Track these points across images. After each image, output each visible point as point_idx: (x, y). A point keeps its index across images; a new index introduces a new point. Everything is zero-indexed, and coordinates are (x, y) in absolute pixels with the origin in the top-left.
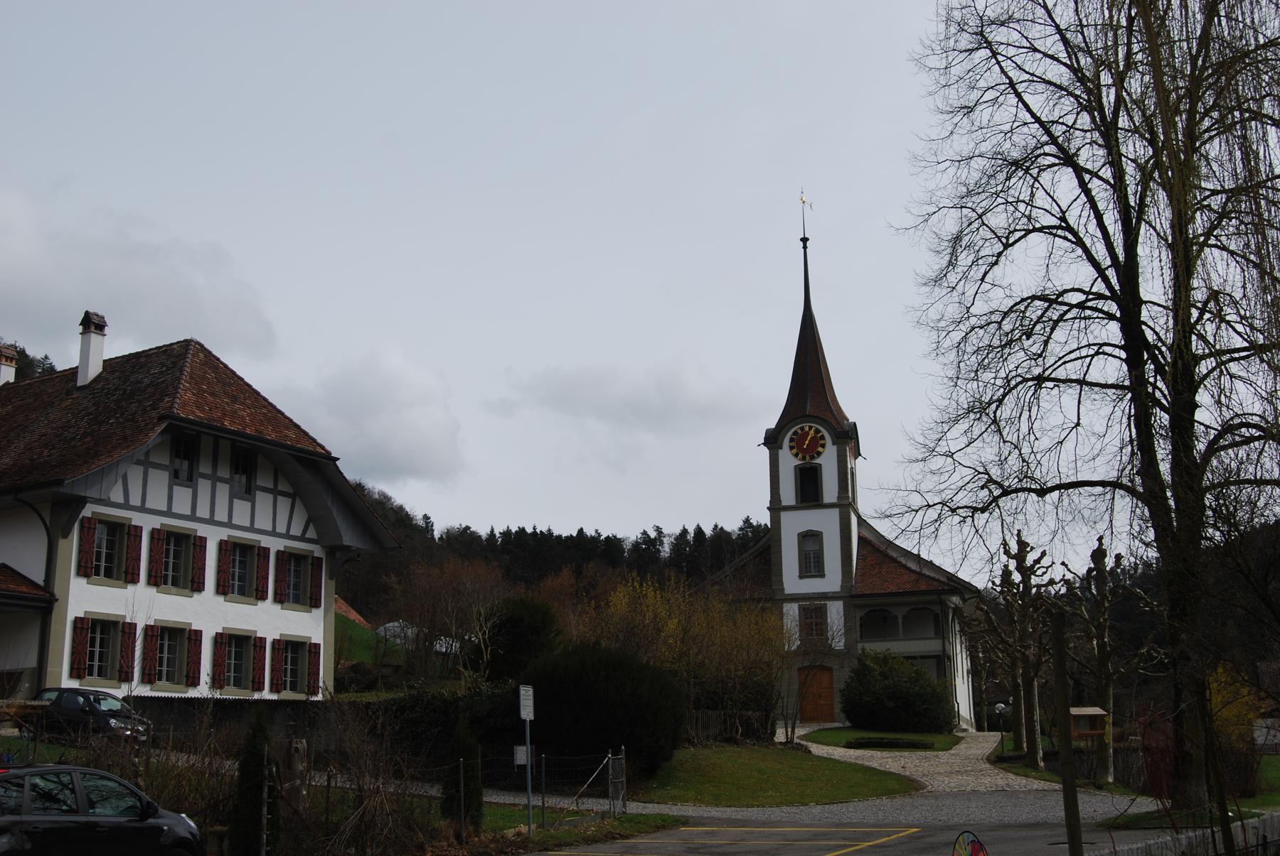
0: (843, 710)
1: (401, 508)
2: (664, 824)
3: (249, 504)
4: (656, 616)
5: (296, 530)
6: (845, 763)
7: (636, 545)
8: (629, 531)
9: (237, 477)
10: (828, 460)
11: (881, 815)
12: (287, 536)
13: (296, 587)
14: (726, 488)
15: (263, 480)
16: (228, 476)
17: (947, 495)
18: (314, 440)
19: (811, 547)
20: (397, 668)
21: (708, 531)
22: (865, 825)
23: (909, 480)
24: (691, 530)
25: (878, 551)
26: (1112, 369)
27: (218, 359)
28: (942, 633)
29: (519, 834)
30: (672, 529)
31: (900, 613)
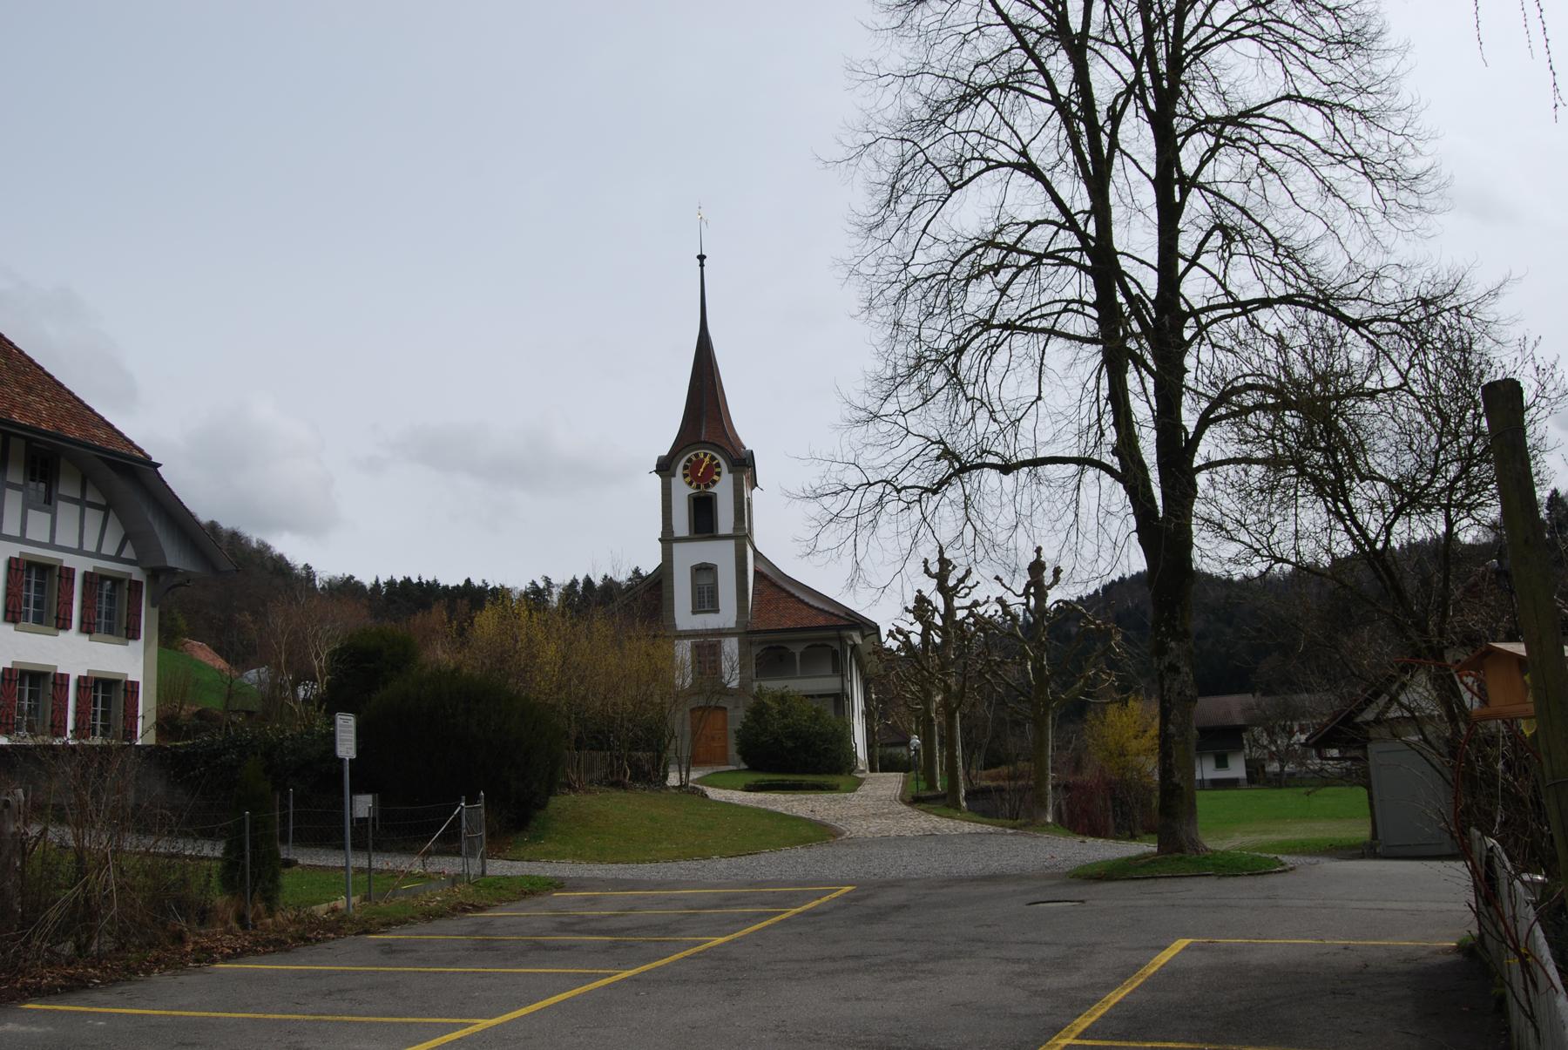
0: (739, 752)
1: (281, 557)
2: (532, 889)
3: (48, 516)
4: (530, 640)
5: (110, 548)
6: (746, 807)
7: (525, 595)
8: (517, 579)
9: (32, 484)
10: (723, 489)
11: (800, 868)
12: (98, 555)
13: (109, 615)
14: (613, 532)
15: (68, 488)
16: (21, 482)
17: (885, 475)
18: (130, 442)
19: (705, 580)
20: (249, 714)
21: (598, 582)
22: (785, 884)
23: (847, 449)
24: (581, 579)
25: (773, 586)
26: (1083, 324)
27: (11, 344)
28: (839, 669)
29: (334, 910)
30: (561, 579)
31: (797, 650)
